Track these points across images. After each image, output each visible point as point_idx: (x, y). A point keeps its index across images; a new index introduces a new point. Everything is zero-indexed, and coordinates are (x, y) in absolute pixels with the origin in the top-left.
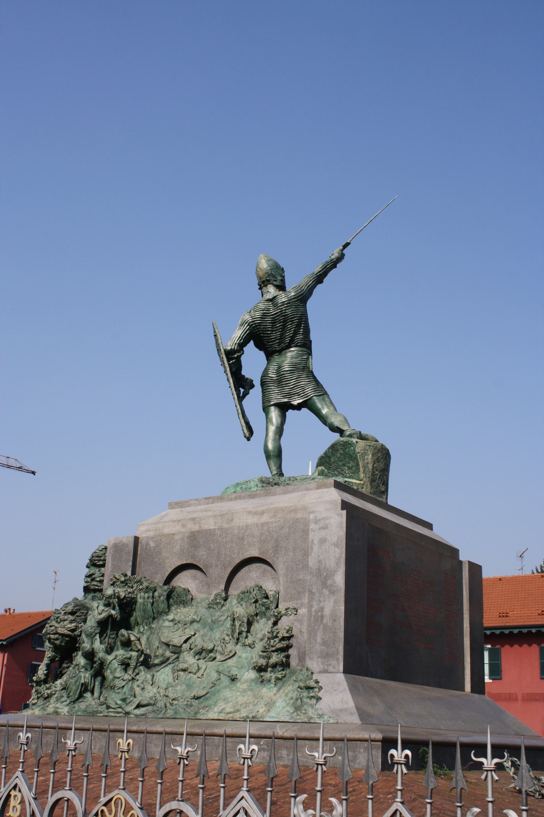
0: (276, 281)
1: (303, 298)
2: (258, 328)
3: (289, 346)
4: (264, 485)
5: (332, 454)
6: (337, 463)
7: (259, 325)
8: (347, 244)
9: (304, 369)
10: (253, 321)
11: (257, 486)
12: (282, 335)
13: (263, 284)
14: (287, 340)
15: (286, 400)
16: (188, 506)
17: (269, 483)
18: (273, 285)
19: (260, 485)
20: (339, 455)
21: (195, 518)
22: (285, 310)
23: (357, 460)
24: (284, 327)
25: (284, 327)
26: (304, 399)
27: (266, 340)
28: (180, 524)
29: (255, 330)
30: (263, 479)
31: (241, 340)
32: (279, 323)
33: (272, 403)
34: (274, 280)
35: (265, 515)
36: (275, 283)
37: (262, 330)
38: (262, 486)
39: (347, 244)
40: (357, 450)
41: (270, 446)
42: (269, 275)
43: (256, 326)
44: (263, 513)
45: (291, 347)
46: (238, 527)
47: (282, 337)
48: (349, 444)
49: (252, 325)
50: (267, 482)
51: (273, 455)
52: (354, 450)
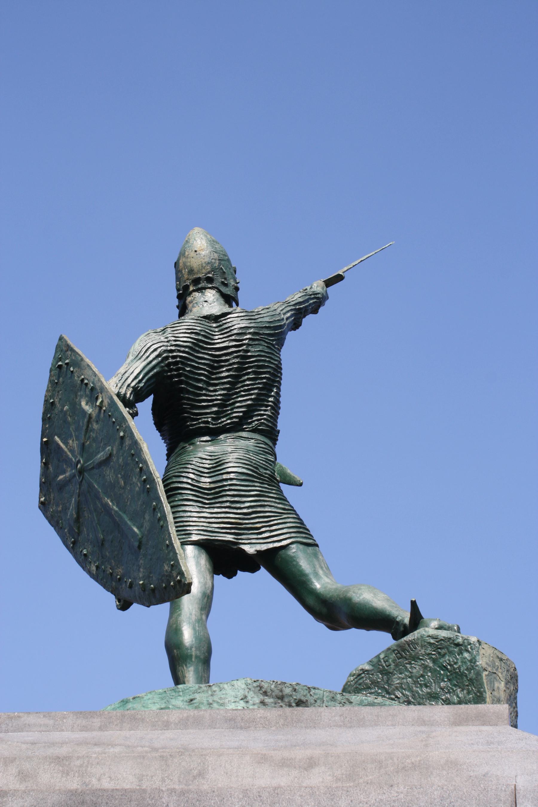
0: (226, 285)
1: (273, 336)
2: (178, 369)
3: (235, 428)
4: (268, 700)
5: (397, 665)
6: (410, 690)
7: (182, 363)
8: (339, 278)
9: (268, 478)
10: (171, 351)
11: (244, 698)
12: (227, 397)
13: (187, 287)
14: (238, 412)
15: (230, 538)
16: (20, 729)
17: (282, 698)
18: (219, 291)
19: (257, 700)
20: (417, 669)
21: (68, 758)
22: (248, 345)
23: (482, 684)
24: (236, 380)
25: (236, 380)
26: (271, 546)
27: (189, 399)
28: (13, 770)
29: (171, 370)
30: (265, 686)
31: (140, 381)
32: (228, 371)
33: (195, 538)
34: (223, 283)
35: (316, 770)
36: (223, 289)
37: (186, 376)
38: (263, 703)
39: (339, 278)
40: (481, 662)
41: (187, 635)
42: (213, 270)
43: (176, 363)
44: (311, 764)
45: (243, 430)
46: (245, 792)
47: (225, 404)
48: (458, 645)
49: (167, 358)
50: (277, 692)
51: (197, 657)
52: (473, 661)
